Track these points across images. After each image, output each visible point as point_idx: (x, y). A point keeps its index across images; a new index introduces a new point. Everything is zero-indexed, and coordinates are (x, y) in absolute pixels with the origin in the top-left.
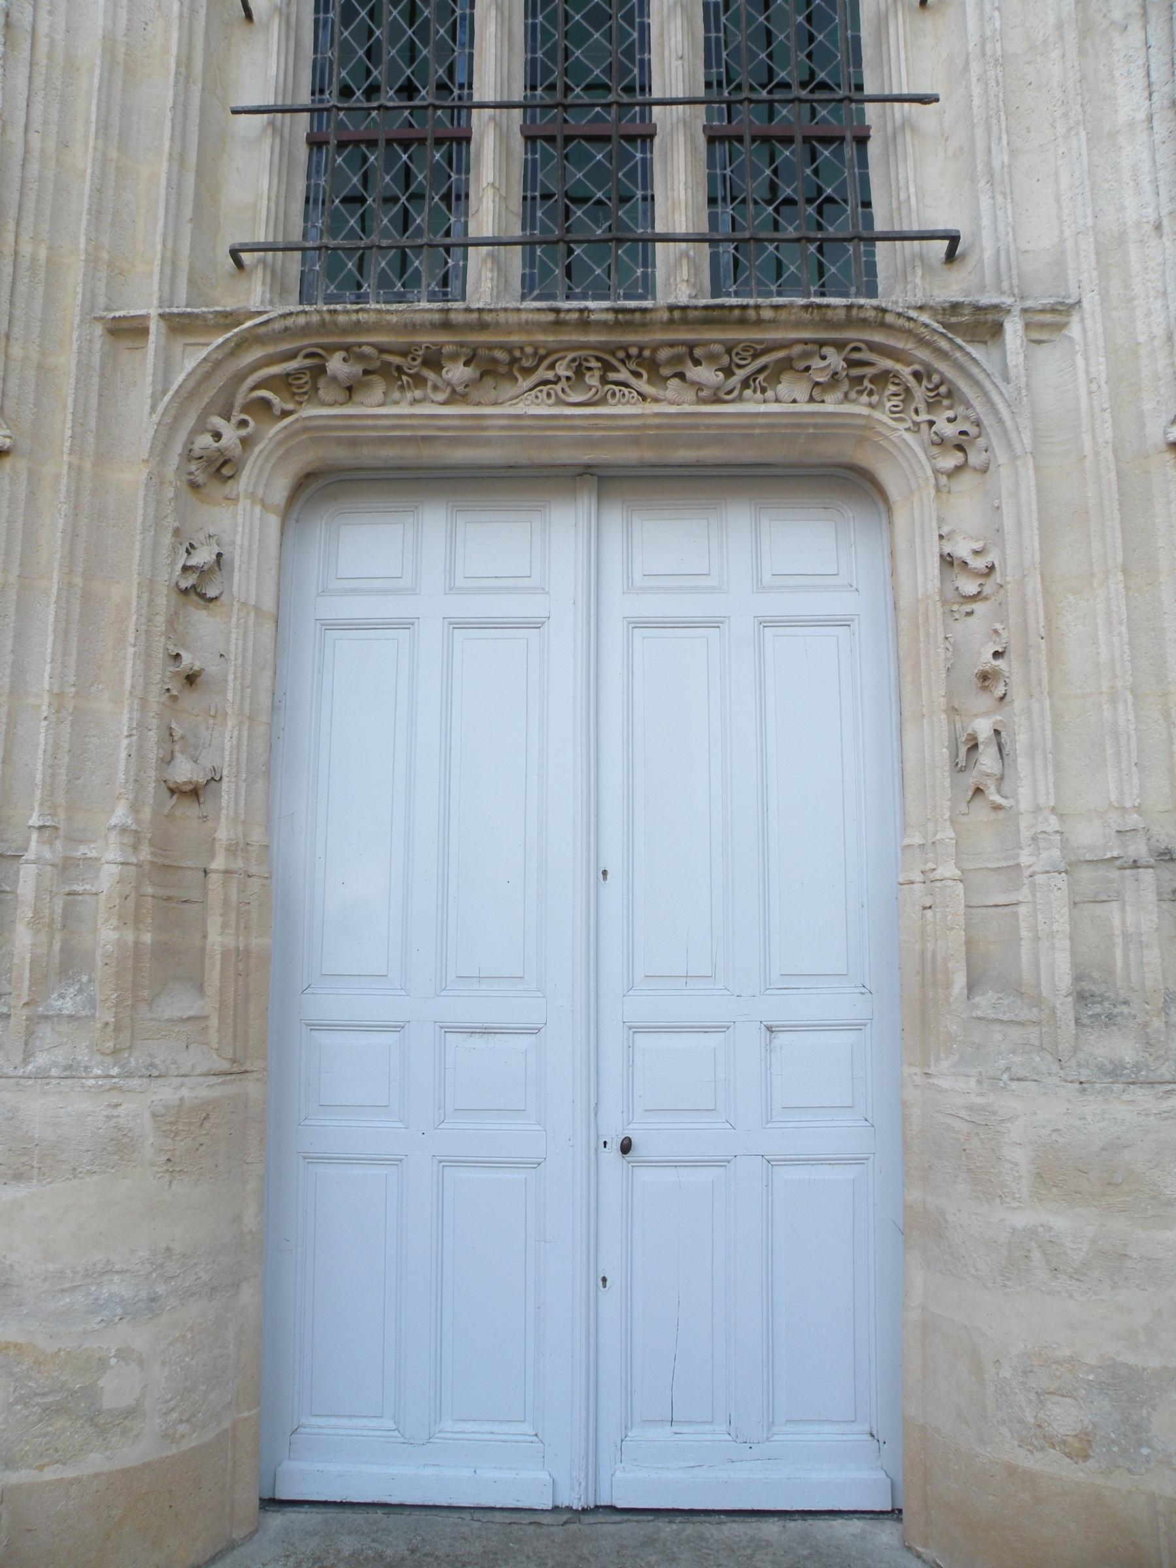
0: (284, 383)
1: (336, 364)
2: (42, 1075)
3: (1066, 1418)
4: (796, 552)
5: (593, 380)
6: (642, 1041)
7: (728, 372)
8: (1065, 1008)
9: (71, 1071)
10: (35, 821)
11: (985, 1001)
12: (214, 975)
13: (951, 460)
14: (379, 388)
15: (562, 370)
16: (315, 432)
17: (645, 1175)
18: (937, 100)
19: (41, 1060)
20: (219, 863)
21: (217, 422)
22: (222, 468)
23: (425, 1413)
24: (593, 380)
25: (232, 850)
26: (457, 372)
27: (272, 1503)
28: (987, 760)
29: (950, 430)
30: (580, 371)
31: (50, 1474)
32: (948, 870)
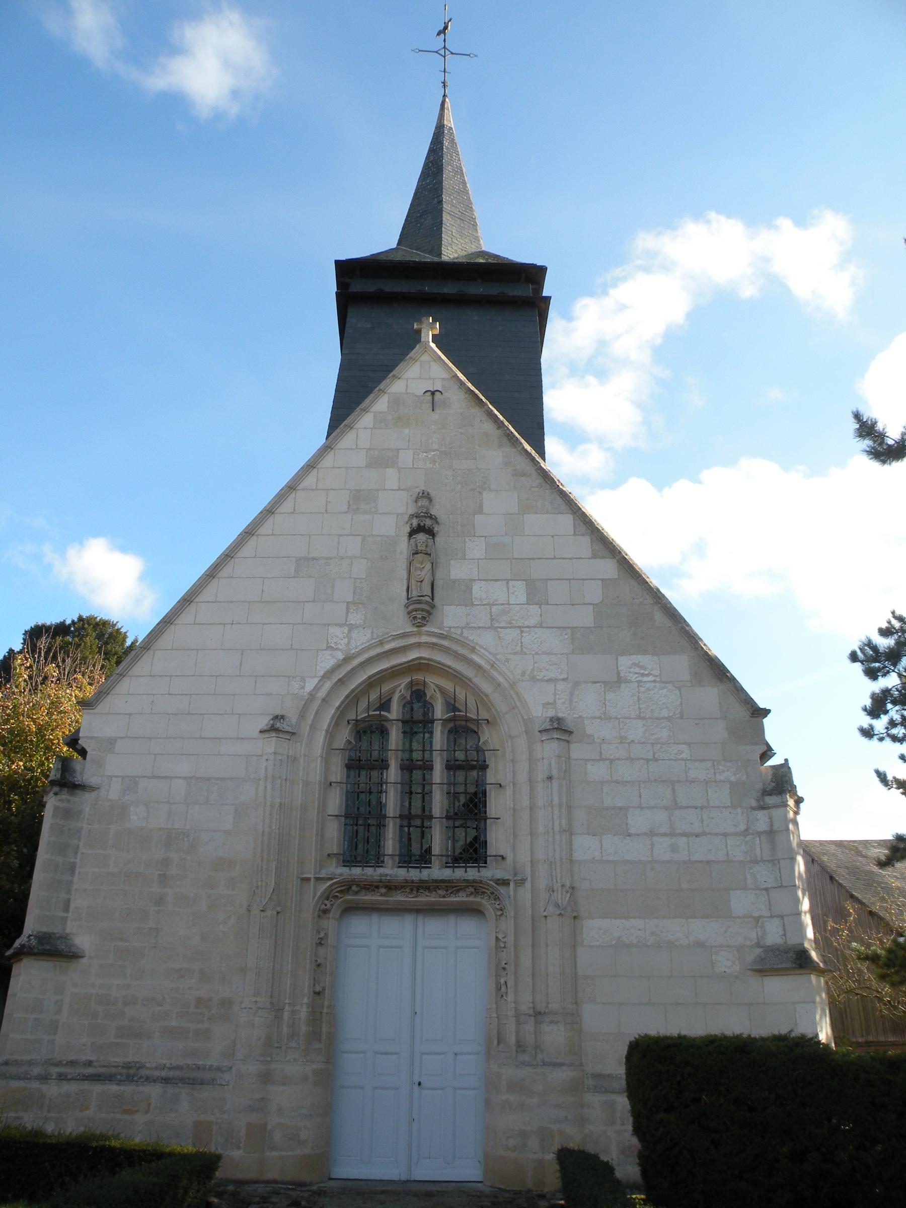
0: (341, 892)
1: (354, 888)
2: (289, 1061)
3: (512, 1142)
4: (467, 926)
5: (415, 892)
6: (424, 1057)
7: (447, 891)
8: (514, 1048)
9: (295, 1060)
10: (287, 1001)
11: (501, 1047)
12: (324, 1037)
13: (499, 913)
14: (363, 892)
15: (407, 890)
16: (346, 901)
17: (424, 1092)
18: (540, 731)
19: (288, 1058)
20: (325, 1011)
21: (326, 902)
22: (325, 912)
23: (372, 1153)
24: (415, 892)
25: (329, 1007)
26: (383, 890)
27: (331, 1179)
28: (503, 989)
29: (498, 907)
30: (412, 890)
31: (290, 1153)
32: (494, 1015)
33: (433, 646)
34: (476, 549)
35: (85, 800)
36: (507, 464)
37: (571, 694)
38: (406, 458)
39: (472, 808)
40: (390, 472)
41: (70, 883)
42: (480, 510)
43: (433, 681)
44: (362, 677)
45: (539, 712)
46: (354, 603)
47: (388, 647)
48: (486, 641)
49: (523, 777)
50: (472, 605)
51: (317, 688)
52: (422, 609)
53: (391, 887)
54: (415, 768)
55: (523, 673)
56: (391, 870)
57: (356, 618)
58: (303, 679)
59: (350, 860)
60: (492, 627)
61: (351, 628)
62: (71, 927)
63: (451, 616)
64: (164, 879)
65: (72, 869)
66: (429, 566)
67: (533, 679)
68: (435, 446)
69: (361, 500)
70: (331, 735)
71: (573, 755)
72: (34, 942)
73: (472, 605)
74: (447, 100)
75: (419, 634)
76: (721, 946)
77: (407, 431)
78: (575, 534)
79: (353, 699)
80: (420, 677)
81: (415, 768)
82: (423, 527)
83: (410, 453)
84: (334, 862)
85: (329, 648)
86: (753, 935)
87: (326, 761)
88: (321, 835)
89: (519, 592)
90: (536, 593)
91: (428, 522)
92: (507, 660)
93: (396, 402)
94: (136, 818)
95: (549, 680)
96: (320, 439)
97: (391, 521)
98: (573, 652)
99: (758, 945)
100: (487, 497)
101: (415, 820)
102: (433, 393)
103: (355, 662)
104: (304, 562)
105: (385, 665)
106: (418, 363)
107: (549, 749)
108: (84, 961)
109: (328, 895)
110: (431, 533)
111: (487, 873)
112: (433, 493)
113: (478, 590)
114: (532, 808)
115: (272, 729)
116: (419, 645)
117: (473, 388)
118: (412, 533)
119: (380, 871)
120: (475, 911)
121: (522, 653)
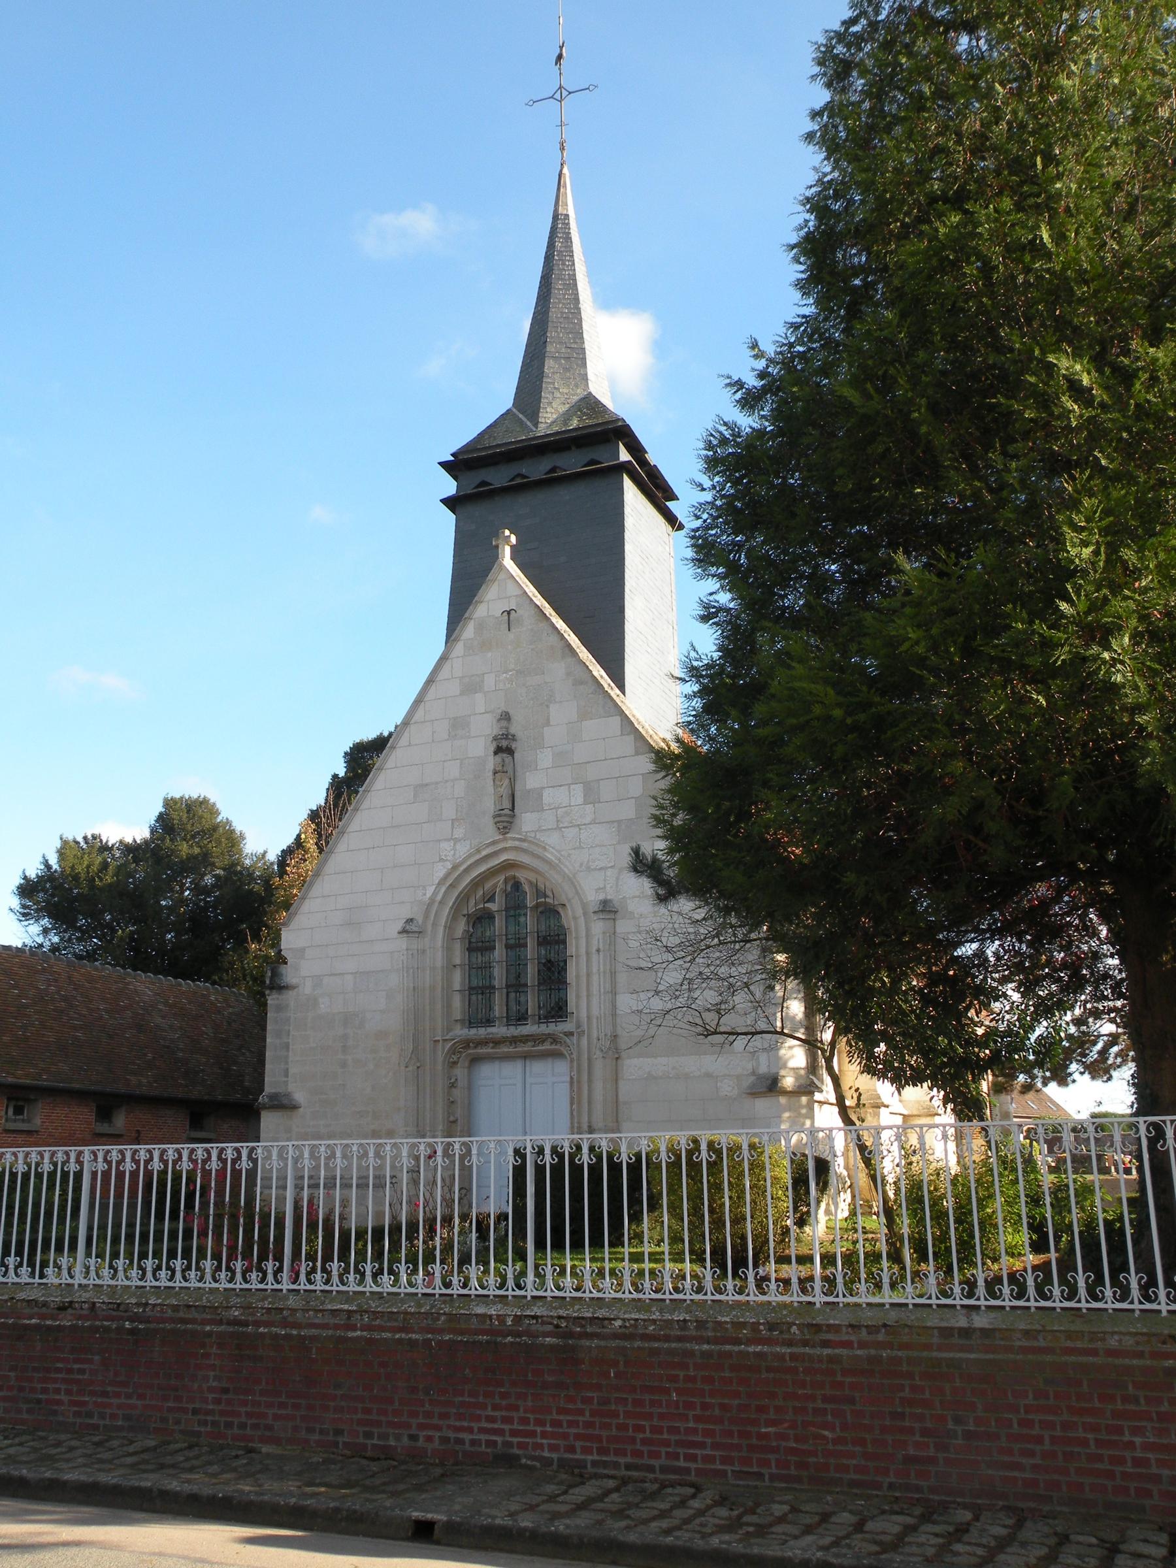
22: (455, 1063)
33: (516, 848)
34: (545, 759)
35: (290, 995)
36: (568, 674)
37: (617, 879)
38: (490, 681)
39: (554, 974)
40: (479, 696)
41: (287, 1057)
42: (548, 723)
43: (522, 875)
44: (467, 880)
45: (593, 897)
46: (457, 819)
47: (484, 853)
48: (552, 840)
49: (583, 951)
50: (543, 810)
51: (435, 893)
52: (506, 819)
53: (497, 1042)
54: (516, 945)
55: (581, 865)
56: (499, 1030)
57: (459, 833)
58: (424, 888)
59: (471, 1023)
60: (558, 828)
61: (456, 841)
62: (291, 1087)
63: (527, 822)
64: (345, 1049)
65: (287, 1047)
66: (506, 782)
67: (589, 869)
68: (513, 666)
69: (459, 725)
70: (450, 928)
71: (618, 930)
72: (266, 1100)
73: (543, 810)
74: (565, 170)
75: (505, 839)
76: (725, 1076)
77: (490, 654)
78: (622, 734)
79: (464, 898)
80: (511, 873)
81: (516, 945)
82: (504, 748)
83: (493, 675)
84: (458, 1026)
85: (441, 860)
86: (750, 1066)
87: (448, 949)
88: (448, 1006)
89: (578, 791)
90: (591, 795)
91: (504, 744)
92: (569, 855)
93: (480, 627)
94: (324, 1006)
95: (601, 869)
96: (440, 647)
97: (480, 747)
98: (619, 843)
99: (753, 1073)
100: (553, 709)
101: (516, 985)
102: (509, 613)
103: (462, 868)
104: (420, 787)
105: (483, 868)
106: (496, 583)
107: (598, 927)
108: (301, 1110)
109: (453, 1051)
110: (510, 751)
111: (568, 1026)
112: (511, 712)
113: (548, 797)
114: (588, 975)
115: (404, 931)
116: (505, 849)
117: (539, 600)
118: (496, 753)
119: (490, 1030)
120: (556, 1055)
121: (581, 848)
